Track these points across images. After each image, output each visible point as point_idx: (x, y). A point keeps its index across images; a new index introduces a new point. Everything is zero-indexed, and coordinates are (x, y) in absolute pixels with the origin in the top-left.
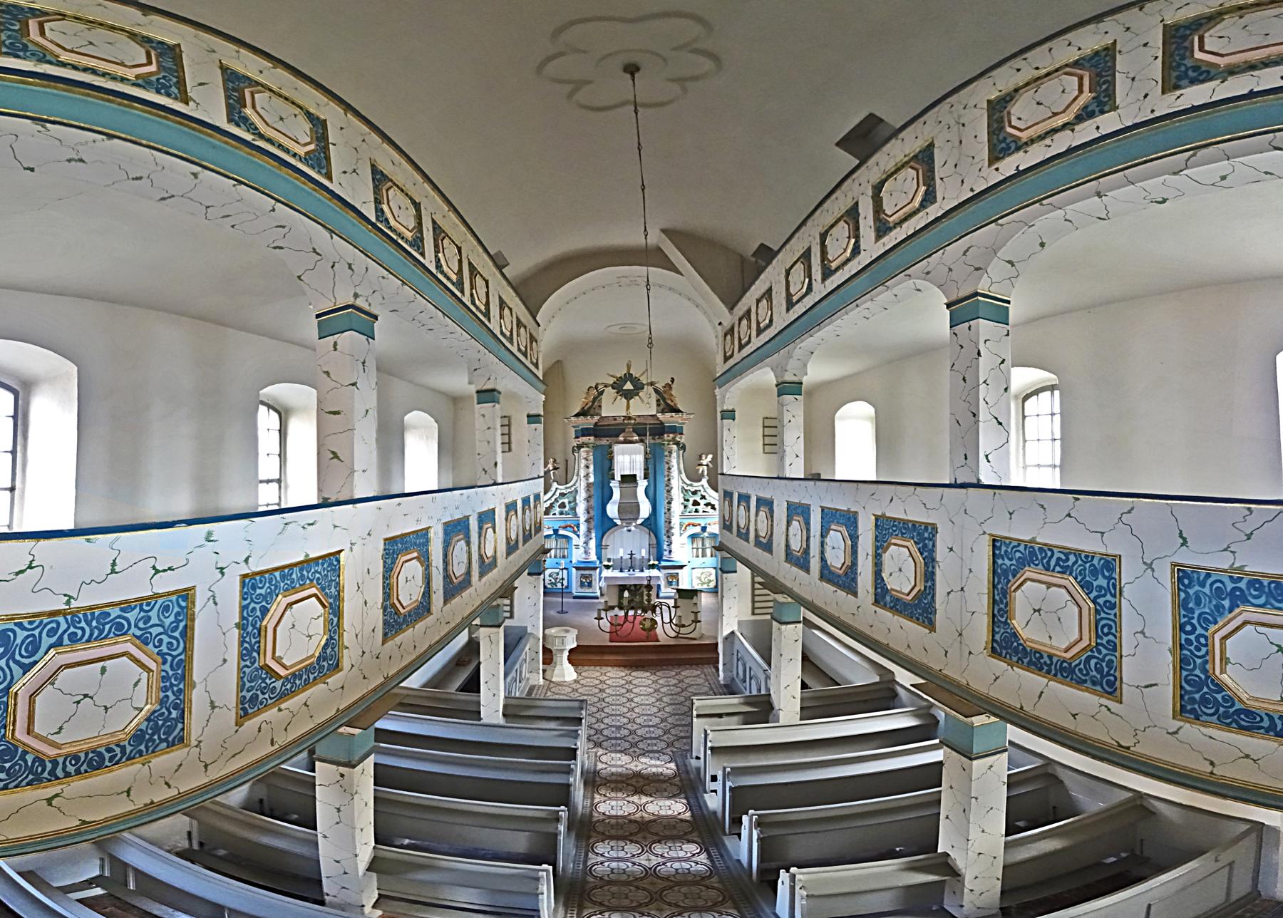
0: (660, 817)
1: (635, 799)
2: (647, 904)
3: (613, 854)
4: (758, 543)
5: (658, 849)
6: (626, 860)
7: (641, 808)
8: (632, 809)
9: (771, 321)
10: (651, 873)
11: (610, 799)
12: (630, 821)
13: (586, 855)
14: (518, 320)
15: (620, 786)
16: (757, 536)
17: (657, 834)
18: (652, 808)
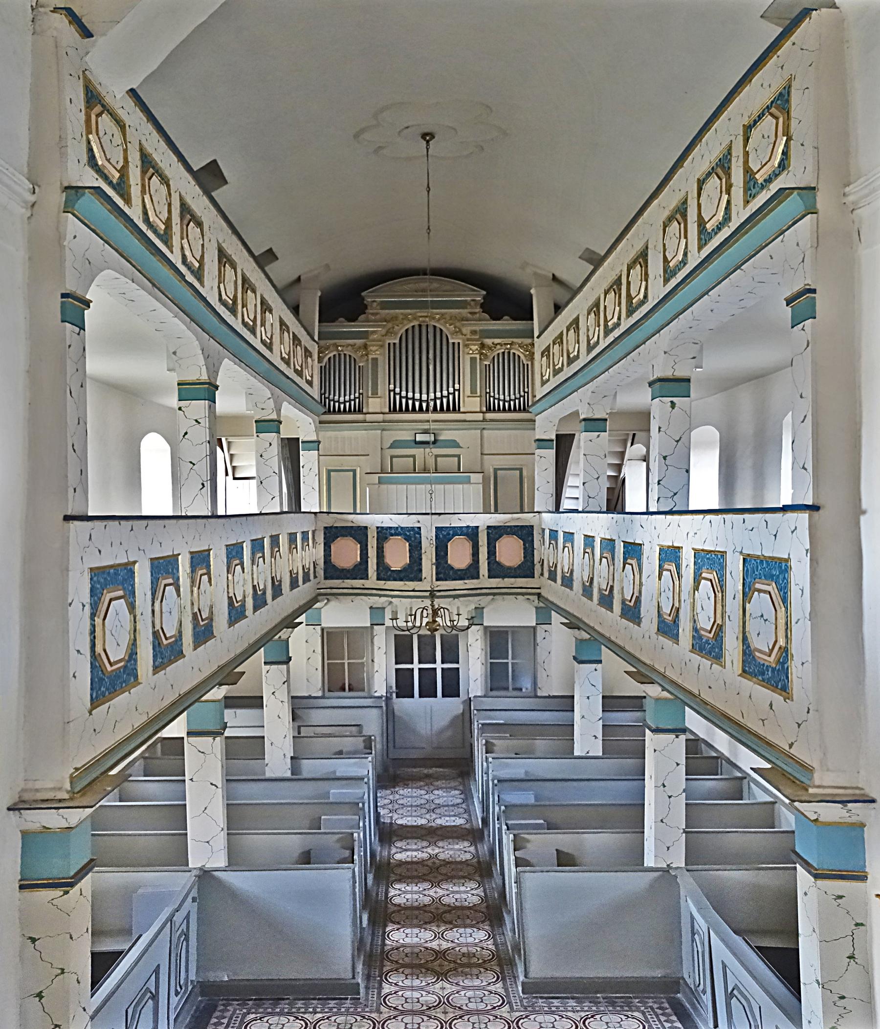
0: (419, 927)
1: (445, 945)
2: (441, 866)
3: (464, 896)
4: (752, 667)
5: (427, 900)
6: (453, 892)
7: (441, 936)
8: (449, 935)
9: (646, 297)
10: (436, 884)
11: (476, 945)
12: (450, 923)
13: (485, 894)
14: (245, 280)
15: (465, 960)
16: (748, 653)
17: (425, 911)
18: (427, 935)
